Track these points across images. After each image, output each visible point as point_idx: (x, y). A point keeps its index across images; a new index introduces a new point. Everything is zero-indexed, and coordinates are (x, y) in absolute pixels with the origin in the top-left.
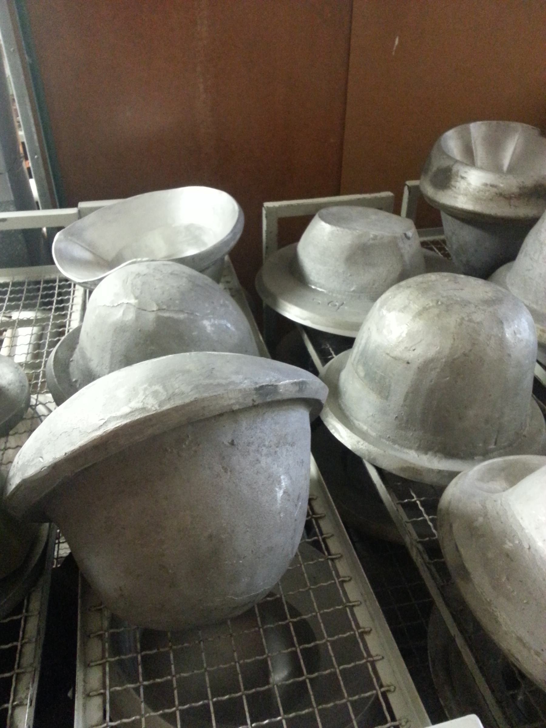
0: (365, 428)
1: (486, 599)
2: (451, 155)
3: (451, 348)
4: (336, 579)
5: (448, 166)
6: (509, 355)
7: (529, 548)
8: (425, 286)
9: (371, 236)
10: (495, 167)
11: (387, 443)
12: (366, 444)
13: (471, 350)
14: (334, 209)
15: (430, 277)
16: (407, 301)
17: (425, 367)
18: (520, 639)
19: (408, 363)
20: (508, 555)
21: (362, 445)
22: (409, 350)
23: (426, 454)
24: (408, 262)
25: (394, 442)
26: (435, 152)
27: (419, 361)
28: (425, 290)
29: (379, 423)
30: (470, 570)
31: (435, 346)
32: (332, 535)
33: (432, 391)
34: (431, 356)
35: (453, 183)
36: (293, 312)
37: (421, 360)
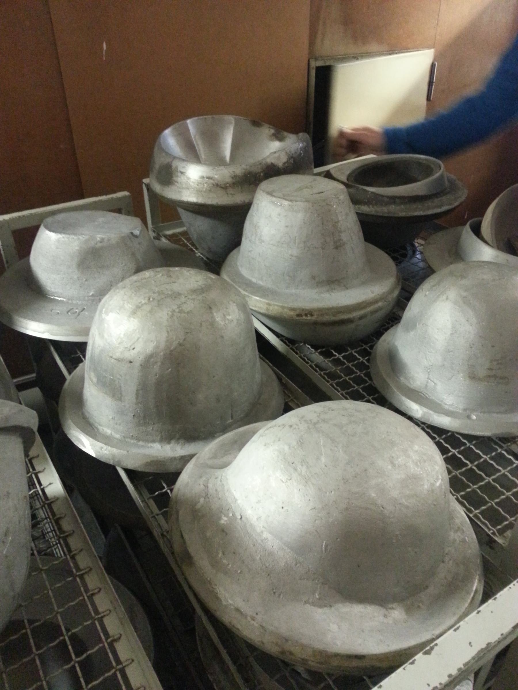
0: (108, 432)
1: (206, 579)
2: (170, 153)
3: (167, 341)
4: (84, 594)
5: (168, 163)
6: (222, 337)
7: (241, 518)
8: (138, 284)
9: (98, 239)
10: (217, 161)
11: (132, 441)
12: (110, 448)
13: (185, 340)
14: (61, 217)
15: (145, 274)
16: (121, 302)
17: (147, 362)
18: (237, 610)
19: (131, 362)
20: (223, 531)
21: (106, 450)
22: (130, 350)
23: (169, 443)
24: (141, 260)
25: (138, 439)
26: (156, 149)
27: (140, 359)
28: (138, 288)
29: (120, 424)
30: (192, 554)
31: (152, 341)
32: (82, 550)
33: (159, 384)
34: (150, 352)
35: (175, 178)
36: (35, 328)
37: (142, 357)
